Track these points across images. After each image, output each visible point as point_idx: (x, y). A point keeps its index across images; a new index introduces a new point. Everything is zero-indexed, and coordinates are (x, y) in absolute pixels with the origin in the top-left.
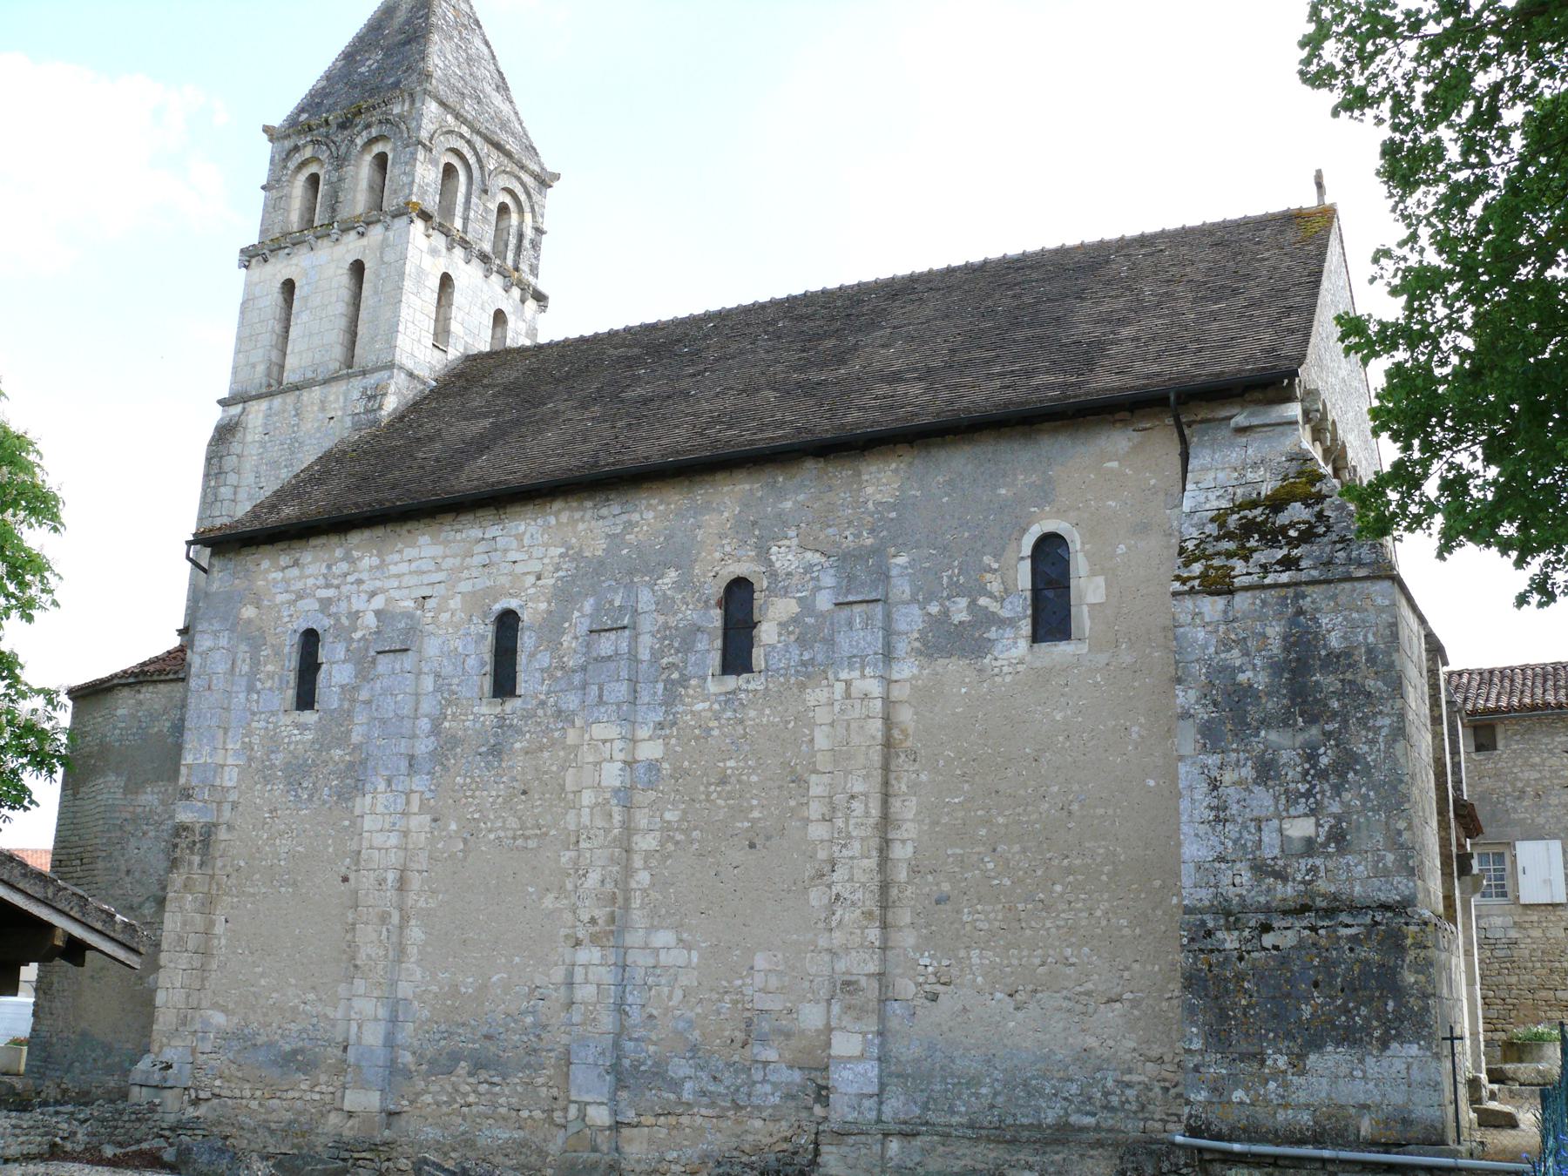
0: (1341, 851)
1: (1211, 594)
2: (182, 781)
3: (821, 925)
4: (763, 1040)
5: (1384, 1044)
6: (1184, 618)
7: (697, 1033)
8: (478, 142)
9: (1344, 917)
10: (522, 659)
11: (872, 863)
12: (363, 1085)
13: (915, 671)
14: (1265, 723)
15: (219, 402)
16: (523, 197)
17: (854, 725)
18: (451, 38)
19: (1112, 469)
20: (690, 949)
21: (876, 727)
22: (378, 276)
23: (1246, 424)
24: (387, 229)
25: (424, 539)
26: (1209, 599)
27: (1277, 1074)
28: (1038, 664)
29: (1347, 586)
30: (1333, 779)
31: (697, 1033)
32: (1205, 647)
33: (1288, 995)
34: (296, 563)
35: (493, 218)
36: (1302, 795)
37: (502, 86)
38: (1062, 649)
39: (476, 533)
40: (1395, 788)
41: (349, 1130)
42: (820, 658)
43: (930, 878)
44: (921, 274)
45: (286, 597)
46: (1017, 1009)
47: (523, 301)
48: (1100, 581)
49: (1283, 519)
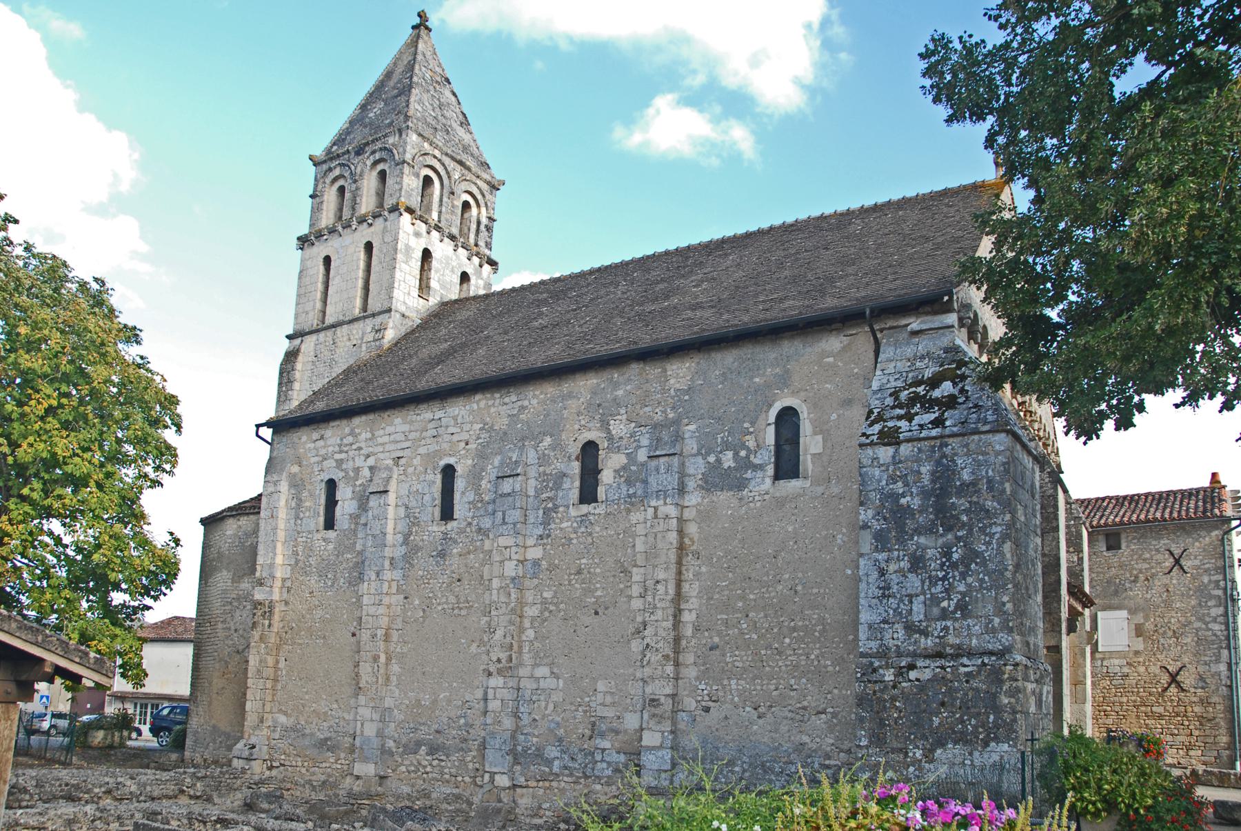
0: (964, 617)
1: (885, 445)
2: (258, 574)
3: (638, 663)
4: (602, 735)
5: (986, 744)
6: (865, 461)
7: (562, 731)
8: (447, 161)
9: (965, 660)
10: (457, 496)
11: (669, 624)
12: (365, 760)
13: (699, 500)
14: (918, 531)
16: (479, 197)
17: (659, 536)
19: (829, 363)
21: (673, 537)
22: (381, 251)
24: (386, 220)
25: (398, 421)
26: (883, 449)
27: (916, 762)
29: (976, 437)
30: (961, 568)
31: (562, 731)
34: (322, 437)
36: (940, 579)
37: (465, 123)
38: (793, 485)
39: (429, 415)
41: (357, 787)
42: (639, 492)
44: (729, 238)
45: (316, 459)
46: (759, 717)
47: (481, 266)
48: (819, 438)
49: (937, 393)
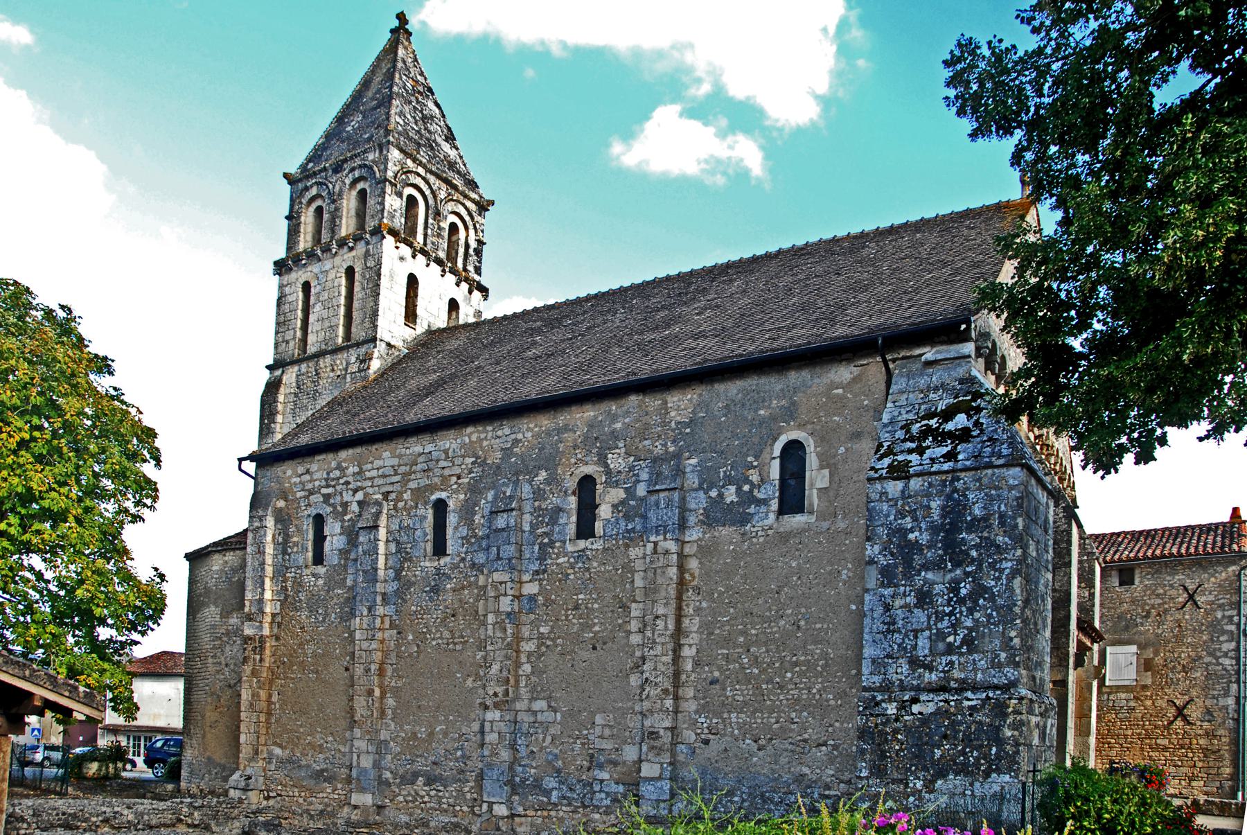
0: (970, 652)
2: (246, 610)
4: (601, 767)
7: (560, 762)
8: (432, 179)
11: (668, 659)
12: (363, 790)
14: (925, 567)
15: (267, 367)
16: (467, 218)
17: (659, 571)
18: (410, 102)
20: (555, 712)
21: (673, 572)
22: (364, 277)
23: (933, 358)
27: (916, 792)
28: (782, 530)
30: (969, 604)
32: (887, 516)
33: (926, 744)
35: (446, 234)
36: (947, 615)
37: (450, 138)
40: (1011, 610)
42: (638, 527)
43: (707, 668)
46: (759, 749)
47: (470, 292)
48: (826, 472)
